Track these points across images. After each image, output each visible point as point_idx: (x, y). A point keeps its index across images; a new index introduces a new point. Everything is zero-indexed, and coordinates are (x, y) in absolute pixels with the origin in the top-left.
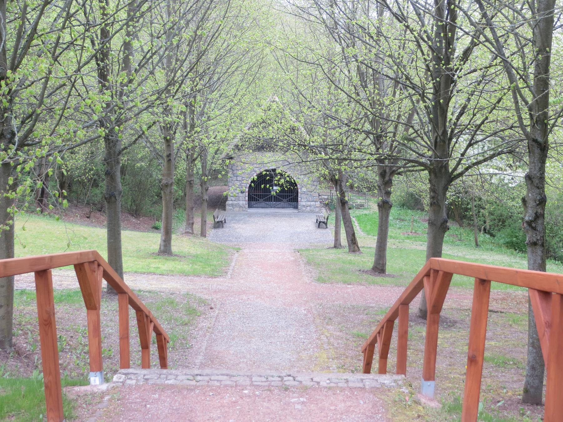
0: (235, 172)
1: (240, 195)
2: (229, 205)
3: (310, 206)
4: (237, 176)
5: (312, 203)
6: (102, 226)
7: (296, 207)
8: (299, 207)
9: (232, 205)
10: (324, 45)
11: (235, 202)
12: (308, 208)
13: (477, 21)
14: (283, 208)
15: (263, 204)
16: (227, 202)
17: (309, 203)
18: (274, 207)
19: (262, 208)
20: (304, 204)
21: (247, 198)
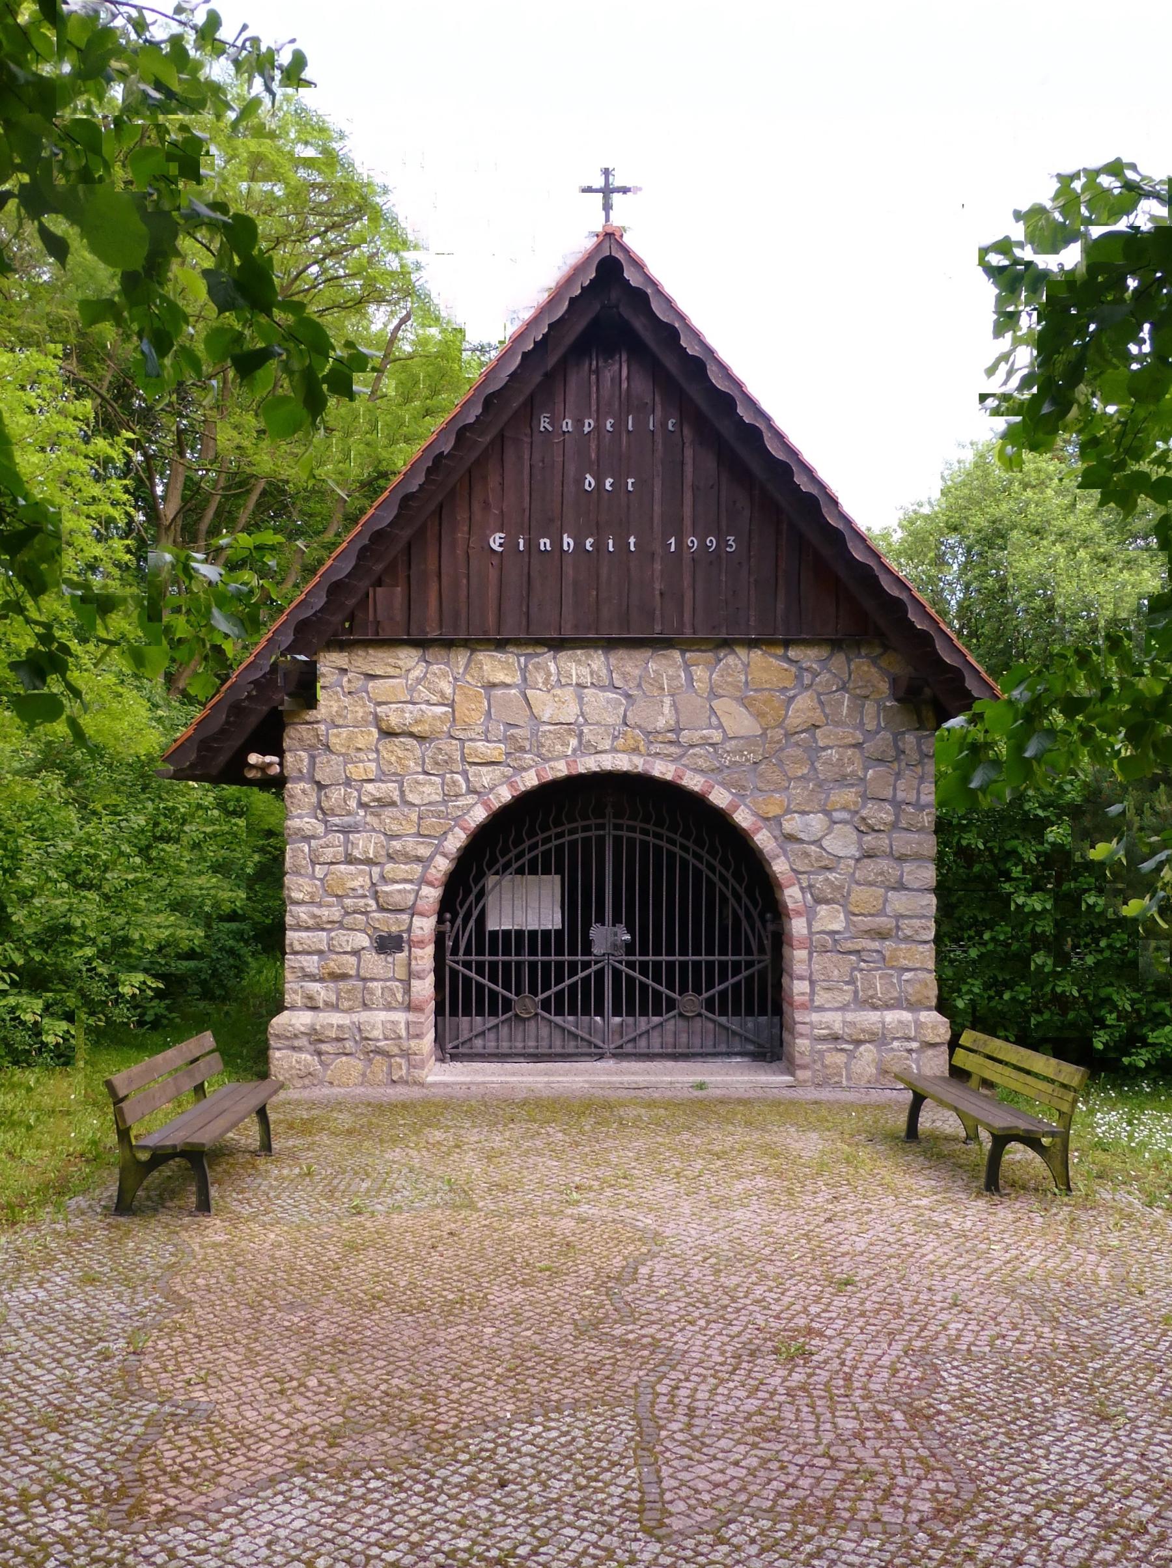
0: (336, 795)
1: (374, 963)
2: (291, 1040)
3: (879, 1038)
4: (346, 831)
5: (891, 1017)
6: (923, 538)
7: (771, 1050)
8: (802, 1045)
9: (315, 1037)
10: (1001, 424)
11: (336, 1018)
12: (868, 1052)
13: (492, 925)
14: (675, 1057)
15: (539, 1032)
16: (280, 1022)
17: (870, 1018)
18: (620, 1055)
19: (536, 1058)
20: (835, 1020)
21: (425, 988)
